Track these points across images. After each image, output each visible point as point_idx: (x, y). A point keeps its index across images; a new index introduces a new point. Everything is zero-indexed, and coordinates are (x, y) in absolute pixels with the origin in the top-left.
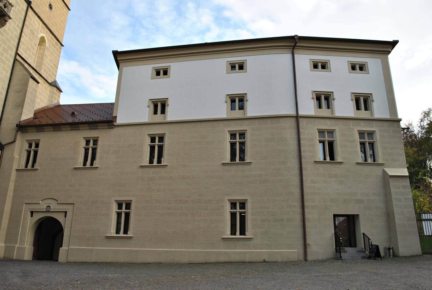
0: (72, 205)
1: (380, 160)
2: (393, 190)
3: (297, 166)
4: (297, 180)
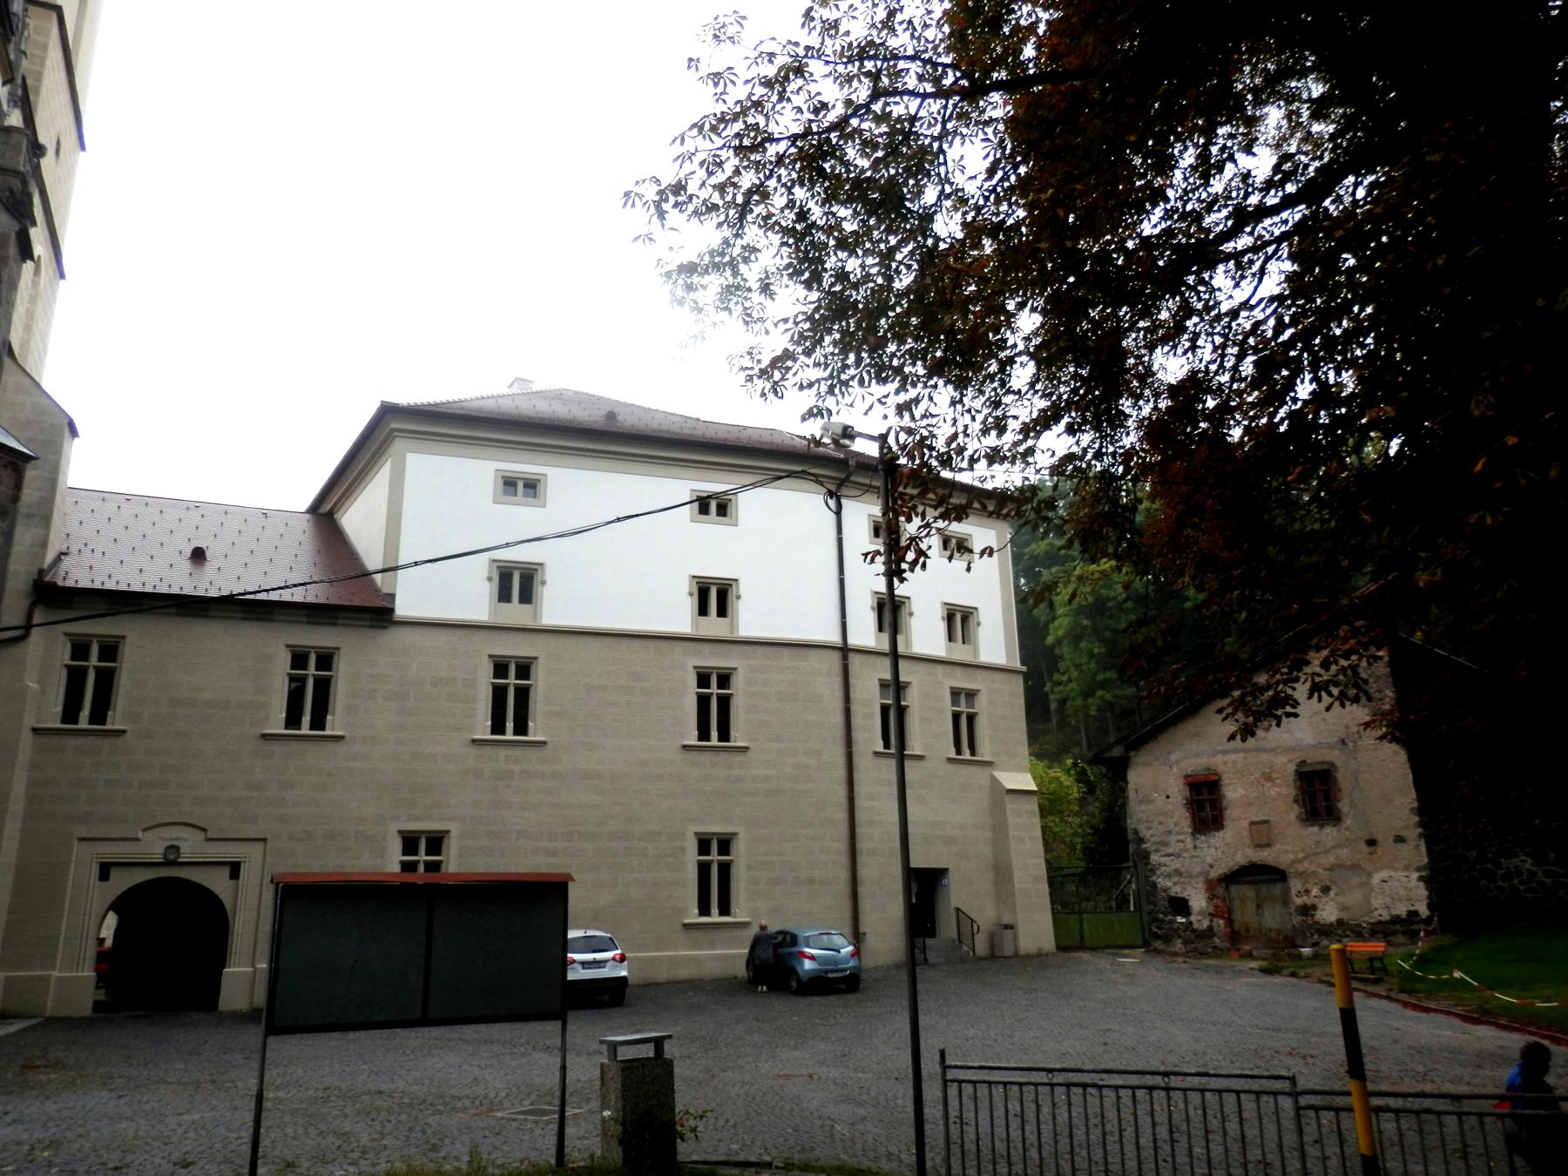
0: (260, 846)
1: (985, 753)
2: (1011, 819)
3: (841, 761)
4: (841, 792)
